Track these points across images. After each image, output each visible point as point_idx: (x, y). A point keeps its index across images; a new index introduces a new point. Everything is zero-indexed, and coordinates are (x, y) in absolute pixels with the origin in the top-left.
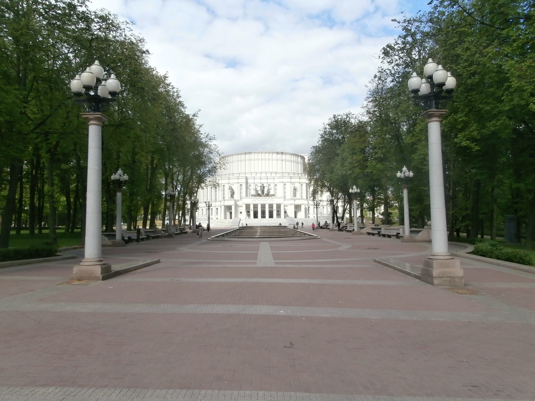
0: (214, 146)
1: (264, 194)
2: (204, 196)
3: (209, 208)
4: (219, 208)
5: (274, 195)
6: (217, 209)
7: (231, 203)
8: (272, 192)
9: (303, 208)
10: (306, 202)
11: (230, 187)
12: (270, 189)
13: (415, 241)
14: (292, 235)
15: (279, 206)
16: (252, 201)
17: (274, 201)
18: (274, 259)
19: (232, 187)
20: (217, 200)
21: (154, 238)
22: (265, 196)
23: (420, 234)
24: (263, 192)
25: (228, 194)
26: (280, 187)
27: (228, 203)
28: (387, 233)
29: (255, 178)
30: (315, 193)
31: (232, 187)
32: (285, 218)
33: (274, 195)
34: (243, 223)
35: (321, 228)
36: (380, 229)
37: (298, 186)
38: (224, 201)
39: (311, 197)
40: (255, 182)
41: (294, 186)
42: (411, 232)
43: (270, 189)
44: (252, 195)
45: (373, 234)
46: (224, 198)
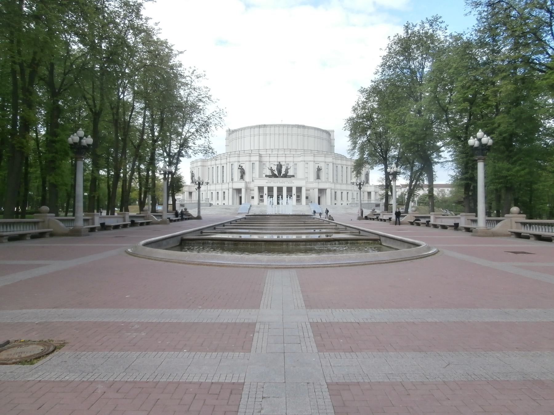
0: (205, 90)
1: (282, 175)
2: (209, 177)
3: (199, 186)
4: (227, 192)
5: (293, 176)
6: (224, 192)
7: (240, 185)
8: (290, 173)
9: (328, 192)
10: (332, 186)
11: (240, 166)
12: (289, 169)
13: (495, 235)
14: (317, 223)
15: (299, 189)
16: (266, 183)
17: (294, 183)
18: (310, 304)
19: (242, 166)
20: (225, 181)
21: (142, 224)
22: (282, 177)
23: (499, 224)
24: (280, 171)
25: (237, 174)
26: (300, 166)
27: (237, 186)
28: (439, 222)
29: (271, 155)
30: (359, 166)
31: (242, 166)
32: (307, 204)
33: (293, 176)
34: (256, 211)
35: (366, 218)
36: (429, 217)
37: (322, 165)
38: (232, 183)
39: (353, 172)
40: (270, 160)
41: (318, 166)
42: (488, 222)
43: (289, 169)
44: (266, 176)
45: (373, 219)
46: (232, 180)
